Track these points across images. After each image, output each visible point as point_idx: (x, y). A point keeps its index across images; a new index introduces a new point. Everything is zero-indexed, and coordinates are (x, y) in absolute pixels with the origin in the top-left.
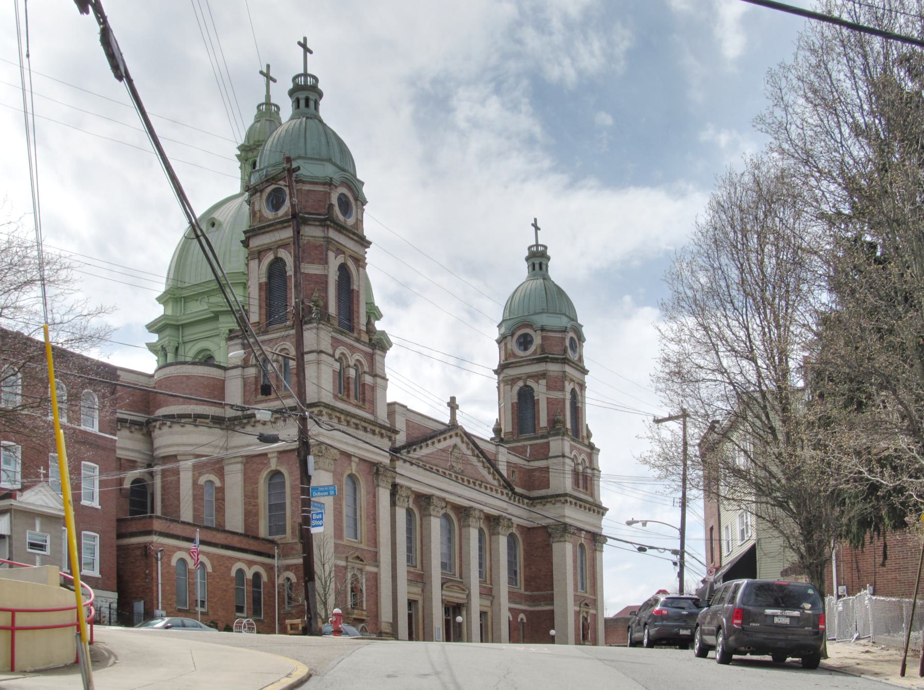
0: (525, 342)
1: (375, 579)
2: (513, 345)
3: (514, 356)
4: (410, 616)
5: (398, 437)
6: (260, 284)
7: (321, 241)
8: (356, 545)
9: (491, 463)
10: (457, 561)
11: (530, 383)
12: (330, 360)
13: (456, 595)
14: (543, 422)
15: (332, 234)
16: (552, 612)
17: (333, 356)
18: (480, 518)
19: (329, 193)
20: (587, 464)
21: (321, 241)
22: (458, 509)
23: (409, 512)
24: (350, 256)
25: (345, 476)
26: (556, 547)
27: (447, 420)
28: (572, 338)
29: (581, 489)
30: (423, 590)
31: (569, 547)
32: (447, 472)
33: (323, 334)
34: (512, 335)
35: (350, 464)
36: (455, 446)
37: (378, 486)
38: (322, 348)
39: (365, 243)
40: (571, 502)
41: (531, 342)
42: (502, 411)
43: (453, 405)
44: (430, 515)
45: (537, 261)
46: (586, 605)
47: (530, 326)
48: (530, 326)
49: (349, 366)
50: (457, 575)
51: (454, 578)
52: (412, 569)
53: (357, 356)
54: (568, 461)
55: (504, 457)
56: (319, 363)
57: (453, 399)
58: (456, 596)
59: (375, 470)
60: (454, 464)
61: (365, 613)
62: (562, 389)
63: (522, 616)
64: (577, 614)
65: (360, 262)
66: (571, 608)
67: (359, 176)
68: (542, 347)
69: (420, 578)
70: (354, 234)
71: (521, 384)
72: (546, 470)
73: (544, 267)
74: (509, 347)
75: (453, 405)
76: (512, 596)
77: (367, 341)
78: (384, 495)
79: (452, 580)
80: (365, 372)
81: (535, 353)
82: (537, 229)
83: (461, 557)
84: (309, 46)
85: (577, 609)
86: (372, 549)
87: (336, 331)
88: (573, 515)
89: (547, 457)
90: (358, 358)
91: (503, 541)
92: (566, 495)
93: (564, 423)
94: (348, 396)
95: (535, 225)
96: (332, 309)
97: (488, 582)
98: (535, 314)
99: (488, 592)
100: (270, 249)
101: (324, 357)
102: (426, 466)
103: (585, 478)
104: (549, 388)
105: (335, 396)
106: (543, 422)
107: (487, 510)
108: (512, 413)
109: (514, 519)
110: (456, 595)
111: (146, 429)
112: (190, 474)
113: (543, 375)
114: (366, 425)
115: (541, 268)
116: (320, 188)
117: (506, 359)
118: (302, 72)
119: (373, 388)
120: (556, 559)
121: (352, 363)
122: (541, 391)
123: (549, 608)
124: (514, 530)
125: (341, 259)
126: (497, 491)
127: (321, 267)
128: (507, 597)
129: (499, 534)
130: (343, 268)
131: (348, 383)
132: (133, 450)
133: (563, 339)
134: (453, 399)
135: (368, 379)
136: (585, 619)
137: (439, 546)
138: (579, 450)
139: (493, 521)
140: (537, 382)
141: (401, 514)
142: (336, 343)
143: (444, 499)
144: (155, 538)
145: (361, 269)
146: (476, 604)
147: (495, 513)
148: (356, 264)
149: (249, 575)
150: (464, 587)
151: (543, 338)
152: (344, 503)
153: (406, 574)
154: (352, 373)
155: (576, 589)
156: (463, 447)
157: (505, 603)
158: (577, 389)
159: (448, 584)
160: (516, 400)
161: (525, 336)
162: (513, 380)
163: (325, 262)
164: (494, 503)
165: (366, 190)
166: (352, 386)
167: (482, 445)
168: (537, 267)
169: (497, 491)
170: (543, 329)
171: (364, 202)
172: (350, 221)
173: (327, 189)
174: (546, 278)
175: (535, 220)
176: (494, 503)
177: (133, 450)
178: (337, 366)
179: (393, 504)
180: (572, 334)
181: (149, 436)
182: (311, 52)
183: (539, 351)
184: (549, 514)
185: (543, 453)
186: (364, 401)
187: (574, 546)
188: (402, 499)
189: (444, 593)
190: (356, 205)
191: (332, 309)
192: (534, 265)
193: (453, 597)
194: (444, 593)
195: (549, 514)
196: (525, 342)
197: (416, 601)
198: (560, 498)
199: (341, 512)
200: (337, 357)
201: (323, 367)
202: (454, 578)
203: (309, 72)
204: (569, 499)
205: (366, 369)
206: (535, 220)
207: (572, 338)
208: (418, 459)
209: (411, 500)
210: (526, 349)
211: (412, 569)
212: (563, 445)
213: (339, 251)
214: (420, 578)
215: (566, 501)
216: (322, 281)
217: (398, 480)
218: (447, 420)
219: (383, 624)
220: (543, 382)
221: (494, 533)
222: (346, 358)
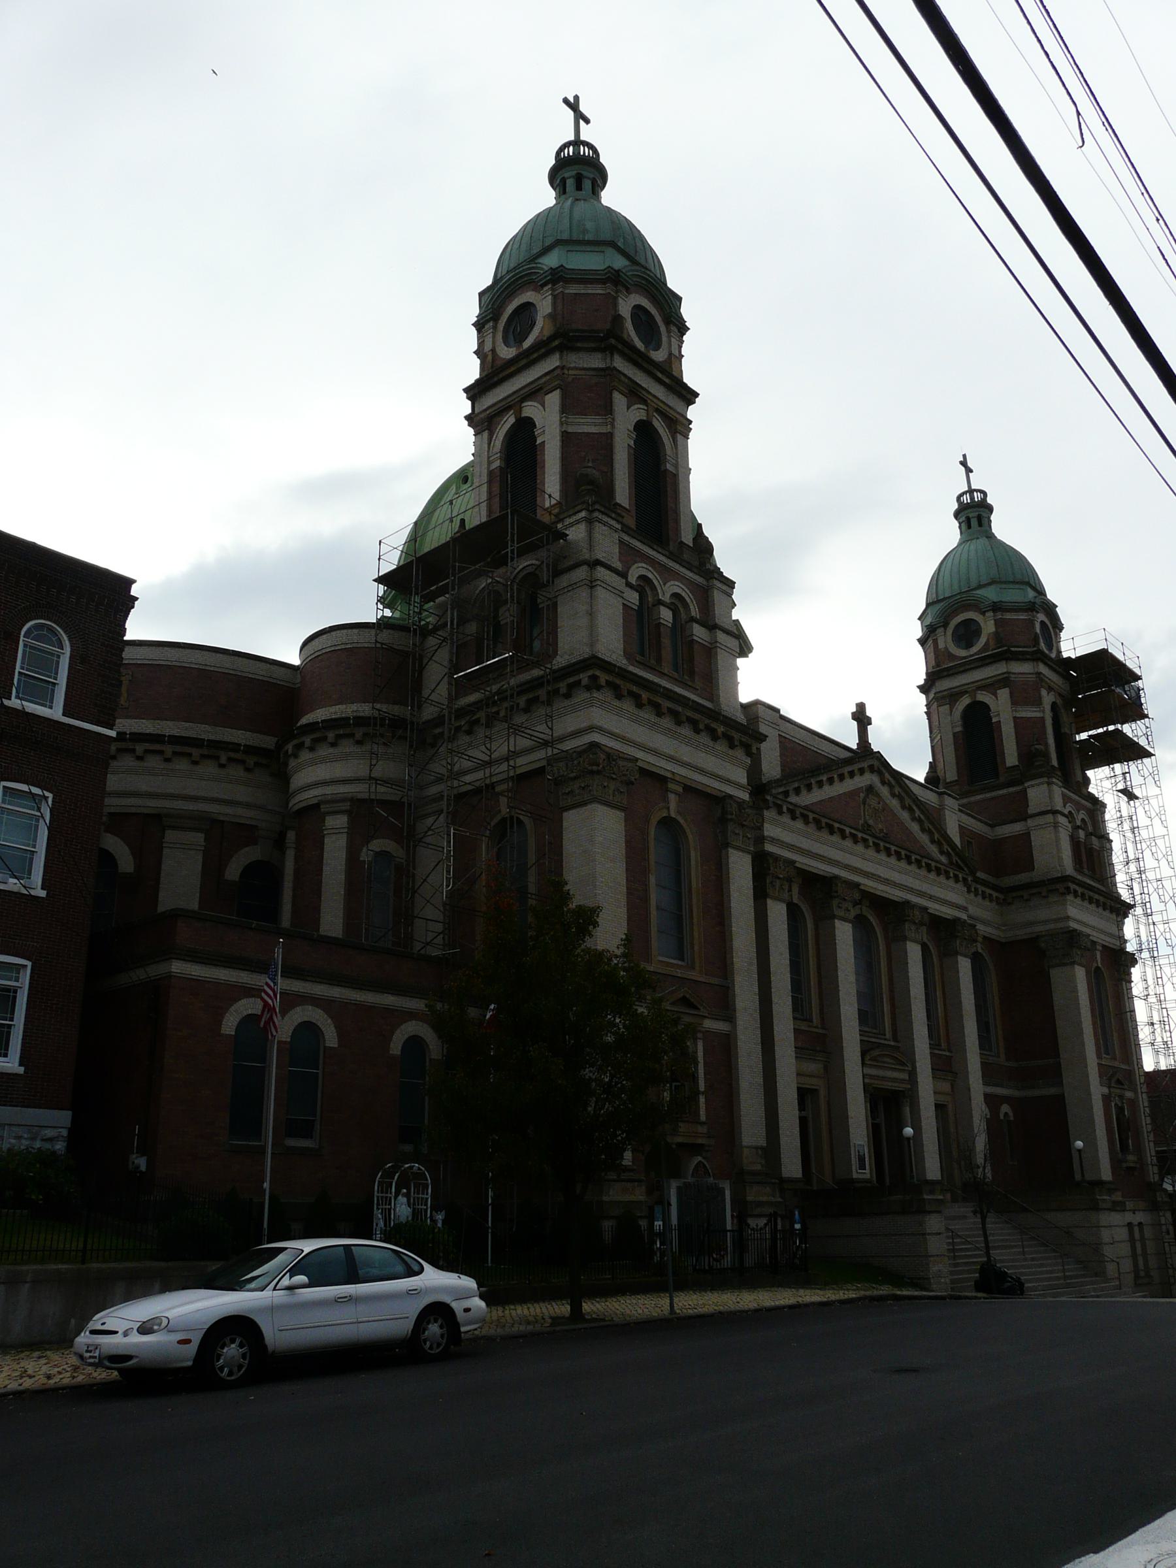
0: (967, 634)
1: (725, 1047)
2: (945, 640)
3: (952, 657)
4: (803, 1122)
5: (763, 746)
6: (491, 473)
7: (1033, 678)
8: (679, 973)
9: (932, 821)
10: (886, 1008)
11: (983, 697)
12: (618, 582)
13: (889, 1074)
14: (1011, 757)
15: (619, 363)
16: (1061, 1099)
17: (623, 575)
18: (922, 924)
19: (615, 298)
20: (1090, 829)
21: (1033, 678)
22: (881, 905)
23: (793, 912)
24: (657, 410)
25: (654, 821)
26: (1056, 974)
27: (852, 742)
28: (1042, 623)
29: (1086, 871)
30: (826, 1068)
31: (1080, 973)
32: (860, 835)
33: (600, 530)
34: (945, 625)
35: (666, 800)
36: (870, 789)
37: (727, 845)
38: (600, 555)
39: (689, 396)
40: (1075, 892)
41: (978, 632)
42: (938, 749)
43: (861, 717)
44: (834, 917)
45: (972, 514)
46: (1119, 1082)
47: (975, 605)
48: (975, 605)
49: (660, 603)
50: (888, 1035)
51: (885, 1043)
52: (803, 1026)
53: (674, 587)
54: (1062, 820)
55: (954, 822)
56: (592, 585)
57: (861, 707)
58: (892, 1077)
59: (715, 806)
60: (871, 822)
61: (703, 1129)
62: (1038, 702)
63: (1005, 1108)
64: (1106, 1099)
65: (681, 427)
66: (1097, 1090)
67: (672, 284)
68: (997, 637)
69: (818, 1043)
70: (663, 372)
71: (966, 701)
72: (1026, 837)
73: (985, 521)
74: (941, 645)
75: (861, 717)
76: (989, 1073)
77: (696, 563)
78: (740, 868)
79: (879, 1045)
80: (693, 620)
81: (986, 647)
82: (969, 471)
83: (892, 999)
84: (583, 108)
85: (1106, 1090)
86: (715, 981)
87: (625, 529)
88: (1081, 916)
89: (1024, 817)
90: (679, 591)
91: (964, 966)
92: (1065, 879)
93: (1046, 755)
94: (659, 660)
95: (964, 463)
96: (623, 493)
97: (944, 1045)
98: (980, 587)
99: (947, 1066)
100: (966, 692)
101: (601, 572)
102: (822, 820)
103: (1090, 851)
104: (1015, 702)
105: (627, 654)
106: (1011, 757)
107: (934, 907)
108: (956, 750)
109: (980, 927)
110: (889, 1074)
111: (274, 765)
112: (342, 841)
113: (1005, 681)
114: (697, 716)
115: (980, 525)
116: (598, 290)
117: (938, 665)
118: (572, 138)
119: (710, 651)
120: (1058, 999)
121: (667, 598)
122: (1001, 706)
123: (1053, 1091)
124: (979, 948)
125: (638, 413)
126: (947, 873)
127: (598, 419)
128: (980, 1074)
129: (957, 953)
130: (643, 430)
131: (659, 635)
132: (248, 805)
133: (1031, 622)
134: (861, 707)
135: (699, 632)
136: (1120, 1110)
137: (852, 978)
138: (1077, 804)
139: (945, 933)
140: (995, 695)
141: (777, 913)
142: (629, 555)
143: (857, 885)
144: (178, 967)
145: (679, 437)
146: (927, 1089)
147: (947, 912)
148: (669, 427)
149: (284, 1028)
150: (906, 1060)
151: (998, 623)
152: (652, 880)
153: (791, 1035)
154: (666, 615)
155: (1099, 1056)
156: (885, 791)
157: (977, 1086)
158: (658, 424)
159: (876, 1053)
160: (959, 729)
161: (968, 622)
162: (951, 695)
163: (607, 409)
164: (946, 897)
165: (686, 311)
166: (666, 642)
167: (915, 789)
168: (974, 522)
169: (947, 873)
170: (996, 607)
171: (682, 329)
172: (659, 356)
173: (609, 289)
174: (990, 536)
175: (964, 456)
176: (946, 897)
177: (248, 805)
178: (633, 597)
179: (760, 894)
180: (1041, 617)
181: (282, 777)
182: (587, 121)
183: (992, 643)
184: (1038, 916)
185: (1019, 810)
186: (692, 673)
187: (1088, 973)
188: (778, 883)
189: (868, 1071)
190: (669, 331)
191: (623, 493)
192: (968, 520)
193: (883, 1078)
194: (868, 1071)
195: (1038, 916)
196: (967, 634)
197: (814, 1092)
198: (1058, 886)
199: (646, 900)
200: (633, 579)
201: (600, 593)
202: (885, 1043)
203: (582, 138)
204: (1073, 886)
205: (695, 611)
206: (964, 456)
207: (1042, 623)
208: (806, 808)
209: (795, 890)
210: (969, 645)
211: (803, 1026)
212: (1050, 791)
213: (635, 394)
214: (818, 1043)
215: (1068, 888)
216: (606, 442)
217: (769, 847)
218: (852, 742)
219: (746, 1151)
220: (1004, 694)
221: (948, 953)
222: (654, 588)
